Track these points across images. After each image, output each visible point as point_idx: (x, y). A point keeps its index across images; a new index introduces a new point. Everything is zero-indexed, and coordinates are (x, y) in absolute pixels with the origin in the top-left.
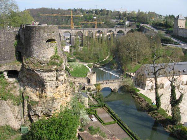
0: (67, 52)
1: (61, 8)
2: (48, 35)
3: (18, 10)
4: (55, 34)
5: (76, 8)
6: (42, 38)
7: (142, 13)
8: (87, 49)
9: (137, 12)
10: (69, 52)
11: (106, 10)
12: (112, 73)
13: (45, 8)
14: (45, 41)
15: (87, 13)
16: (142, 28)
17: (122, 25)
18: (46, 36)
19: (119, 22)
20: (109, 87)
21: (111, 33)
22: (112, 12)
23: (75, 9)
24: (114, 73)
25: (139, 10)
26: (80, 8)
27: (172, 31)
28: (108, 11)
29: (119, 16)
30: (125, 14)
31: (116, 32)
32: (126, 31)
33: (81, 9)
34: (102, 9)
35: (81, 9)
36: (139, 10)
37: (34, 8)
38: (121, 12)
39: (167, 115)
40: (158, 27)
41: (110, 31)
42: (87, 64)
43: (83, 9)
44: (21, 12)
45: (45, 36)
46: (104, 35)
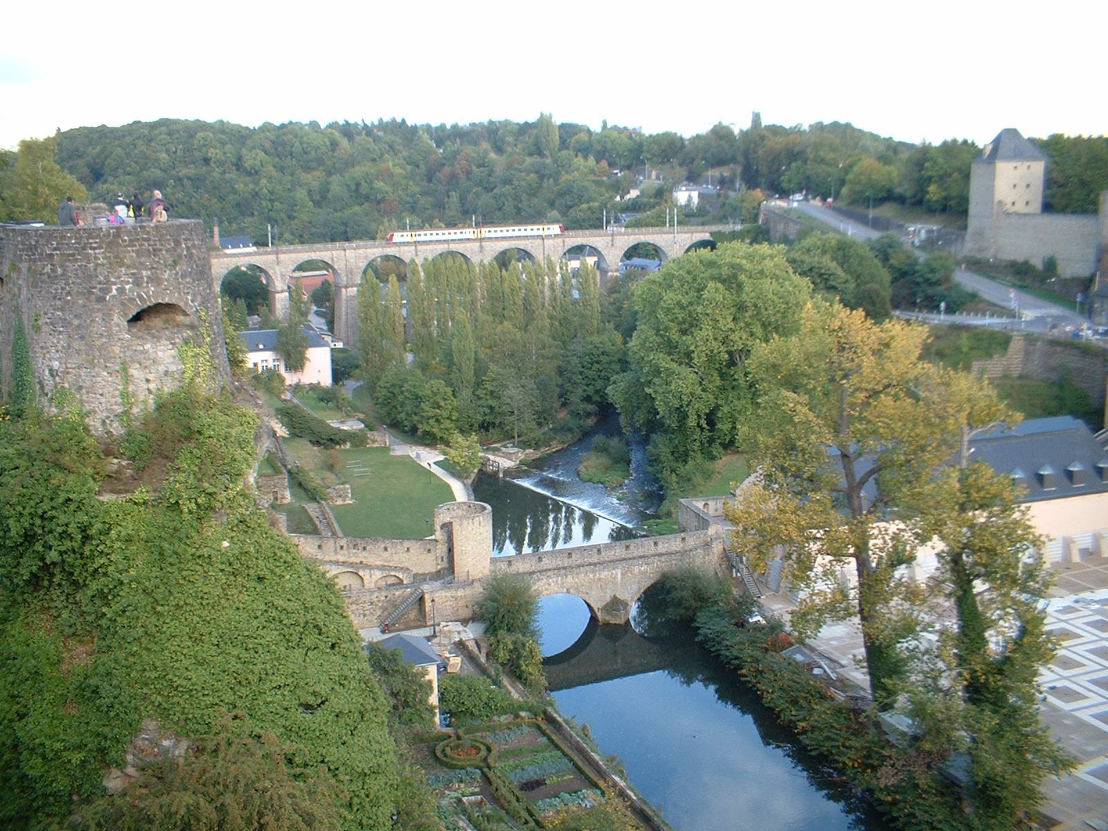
2: (137, 283)
4: (183, 276)
6: (101, 300)
7: (1057, 143)
14: (119, 320)
15: (440, 143)
17: (653, 209)
18: (130, 289)
21: (591, 261)
25: (756, 118)
29: (669, 151)
32: (675, 242)
36: (756, 118)
37: (110, 125)
38: (806, 127)
39: (1040, 648)
41: (577, 251)
44: (647, 135)
45: (121, 291)
46: (922, 513)
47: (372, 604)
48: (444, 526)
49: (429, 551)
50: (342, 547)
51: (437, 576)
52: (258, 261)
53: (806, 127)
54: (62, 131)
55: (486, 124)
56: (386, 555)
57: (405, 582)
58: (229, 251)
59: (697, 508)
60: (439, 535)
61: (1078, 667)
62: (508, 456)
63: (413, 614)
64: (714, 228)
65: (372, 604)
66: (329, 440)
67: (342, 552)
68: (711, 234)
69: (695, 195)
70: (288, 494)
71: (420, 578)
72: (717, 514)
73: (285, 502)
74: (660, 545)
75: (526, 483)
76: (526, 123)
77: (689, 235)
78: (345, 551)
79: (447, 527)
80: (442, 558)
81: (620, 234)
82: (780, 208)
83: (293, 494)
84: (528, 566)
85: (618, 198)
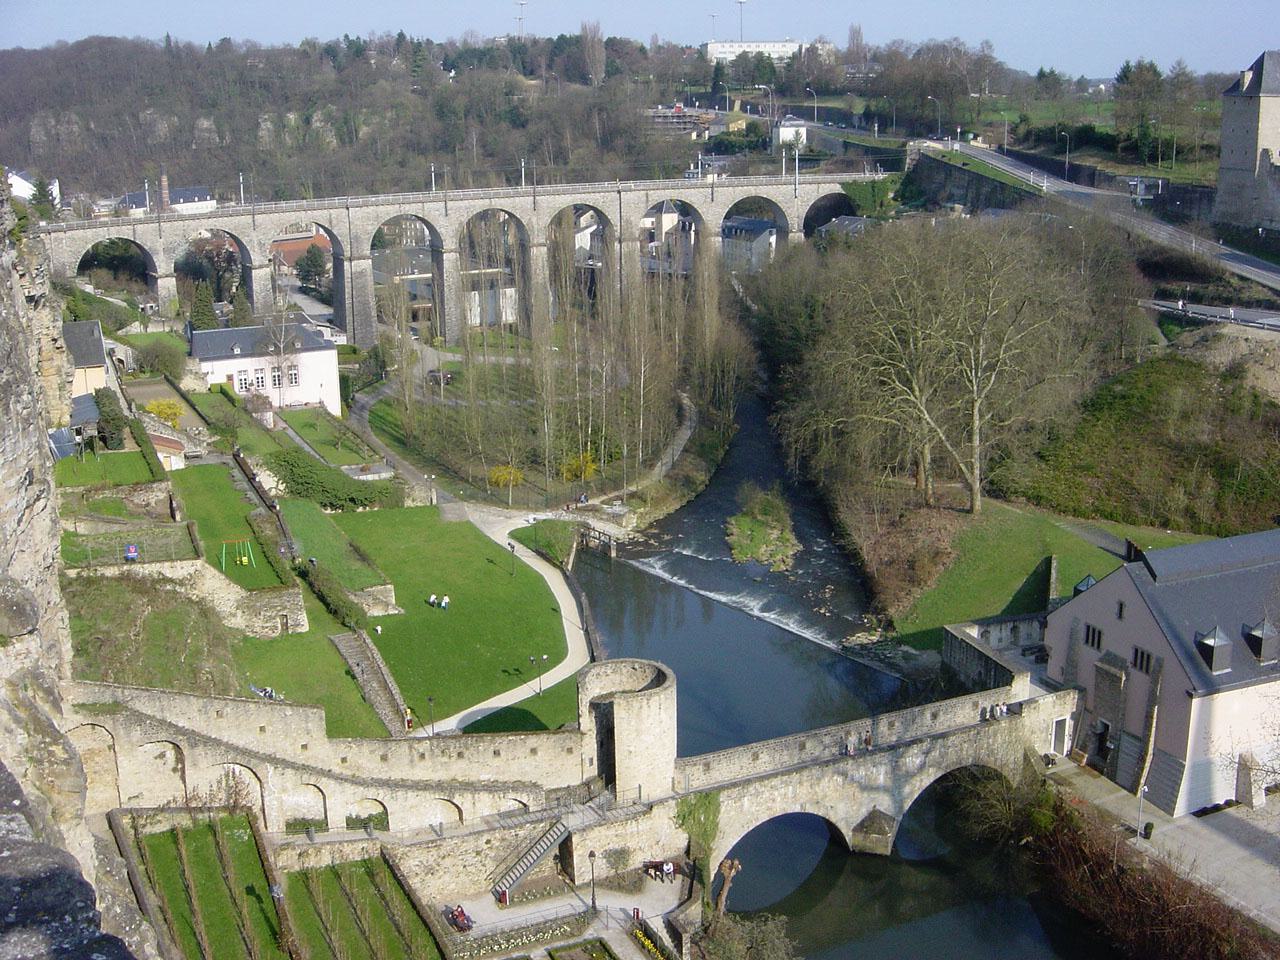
0: (320, 411)
1: (238, 37)
3: (639, 869)
5: (360, 32)
8: (485, 361)
9: (841, 42)
10: (335, 407)
11: (606, 34)
12: (765, 608)
13: (110, 41)
16: (929, 165)
17: (751, 150)
19: (715, 131)
20: (810, 809)
22: (642, 50)
23: (351, 43)
24: (786, 611)
25: (855, 34)
26: (395, 34)
27: (1206, 194)
28: (612, 44)
30: (754, 68)
31: (713, 216)
33: (401, 36)
34: (572, 30)
35: (401, 36)
36: (855, 34)
37: (24, 47)
40: (1067, 158)
42: (523, 520)
43: (414, 34)
47: (478, 853)
48: (594, 706)
49: (570, 751)
50: (422, 756)
51: (584, 793)
52: (225, 224)
53: (883, 46)
54: (660, 43)
55: (555, 38)
56: (497, 761)
57: (531, 809)
58: (183, 208)
59: (970, 637)
60: (588, 722)
61: (1207, 663)
62: (616, 519)
63: (549, 866)
64: (848, 177)
65: (478, 853)
66: (348, 499)
67: (422, 764)
68: (843, 185)
69: (803, 131)
70: (303, 618)
71: (562, 798)
72: (1004, 644)
73: (299, 630)
74: (941, 718)
75: (656, 568)
76: (562, 38)
77: (815, 186)
78: (428, 762)
79: (604, 714)
80: (591, 760)
81: (722, 185)
82: (934, 150)
83: (312, 620)
84: (737, 767)
85: (694, 136)
